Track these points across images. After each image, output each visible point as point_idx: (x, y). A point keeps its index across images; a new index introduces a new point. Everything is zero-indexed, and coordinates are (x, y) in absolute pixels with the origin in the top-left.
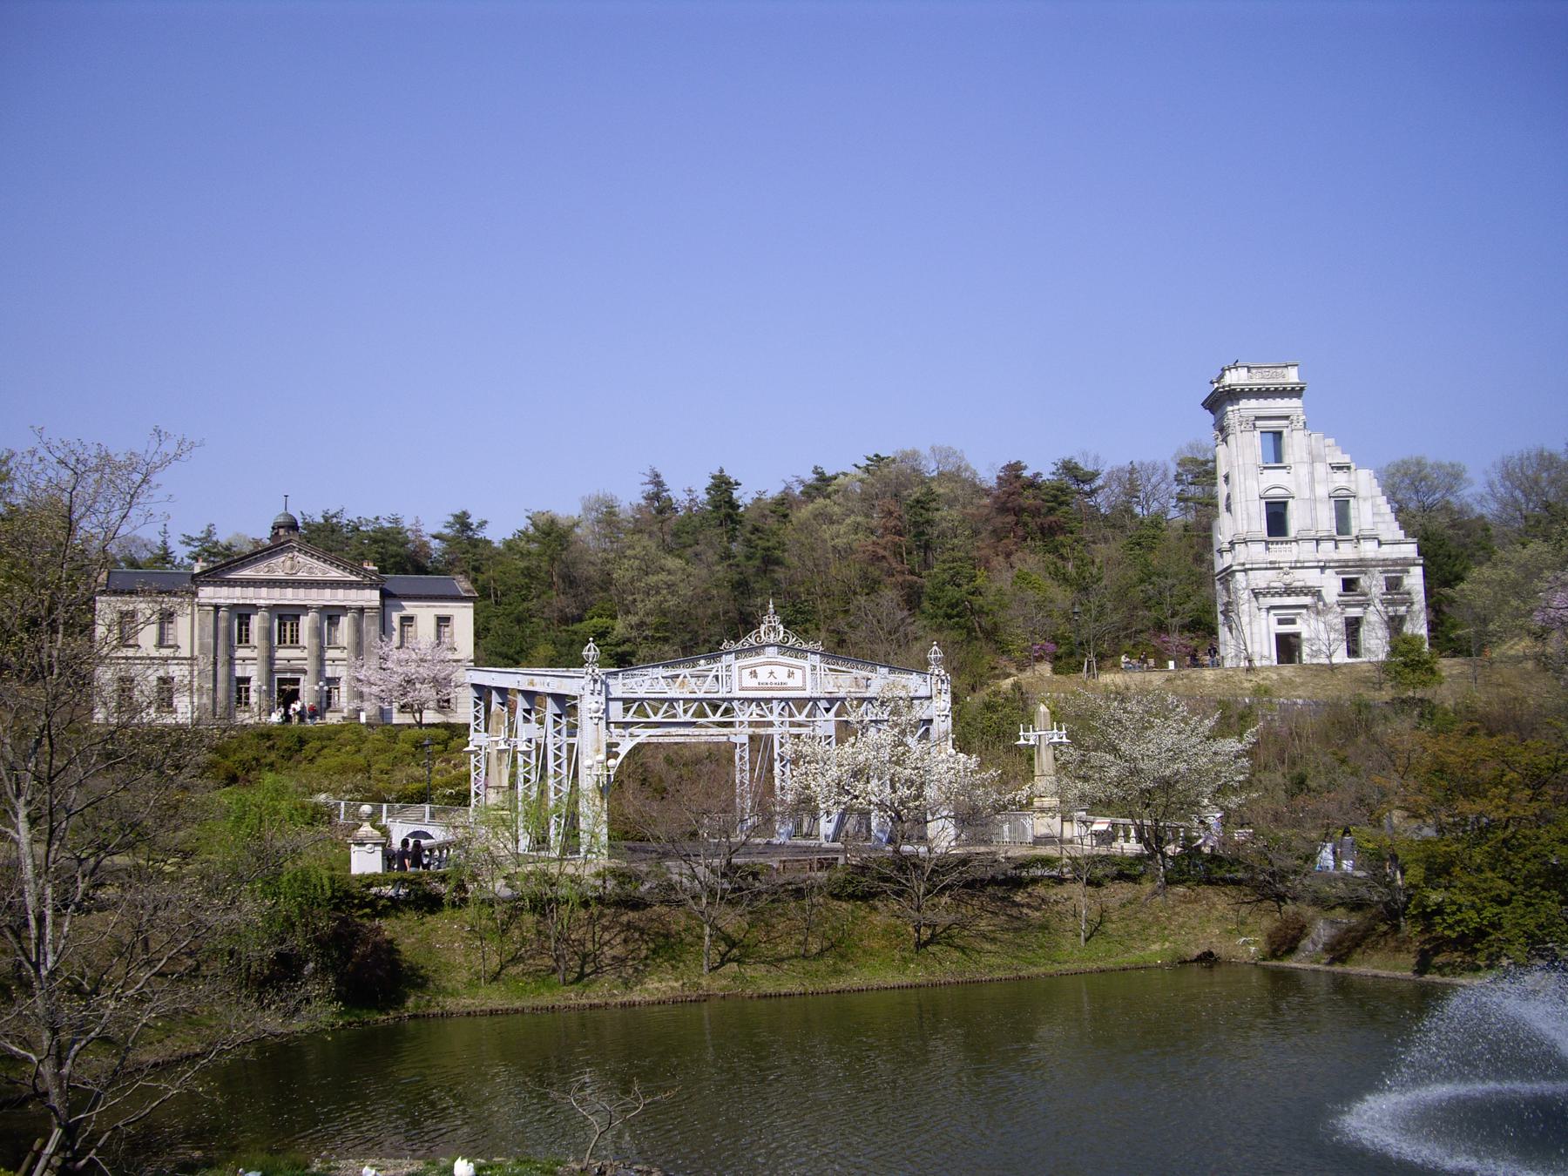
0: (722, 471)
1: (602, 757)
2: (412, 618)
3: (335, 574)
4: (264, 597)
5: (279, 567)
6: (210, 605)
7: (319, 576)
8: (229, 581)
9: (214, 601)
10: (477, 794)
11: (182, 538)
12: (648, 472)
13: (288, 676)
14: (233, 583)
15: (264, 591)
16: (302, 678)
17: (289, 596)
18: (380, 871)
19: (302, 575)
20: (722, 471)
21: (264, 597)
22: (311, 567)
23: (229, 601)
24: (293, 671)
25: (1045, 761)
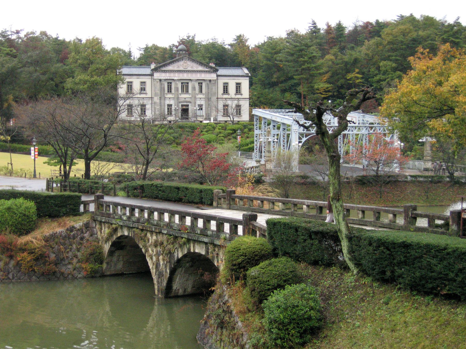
0: (340, 22)
1: (297, 143)
2: (240, 114)
3: (200, 68)
4: (176, 76)
5: (180, 65)
6: (158, 79)
7: (195, 69)
8: (164, 71)
9: (159, 78)
10: (340, 147)
11: (138, 48)
12: (311, 22)
13: (185, 104)
14: (165, 71)
15: (177, 74)
16: (190, 104)
17: (185, 76)
18: (347, 32)
19: (189, 69)
20: (340, 22)
21: (176, 76)
22: (191, 66)
23: (164, 78)
24: (186, 102)
25: (427, 148)
